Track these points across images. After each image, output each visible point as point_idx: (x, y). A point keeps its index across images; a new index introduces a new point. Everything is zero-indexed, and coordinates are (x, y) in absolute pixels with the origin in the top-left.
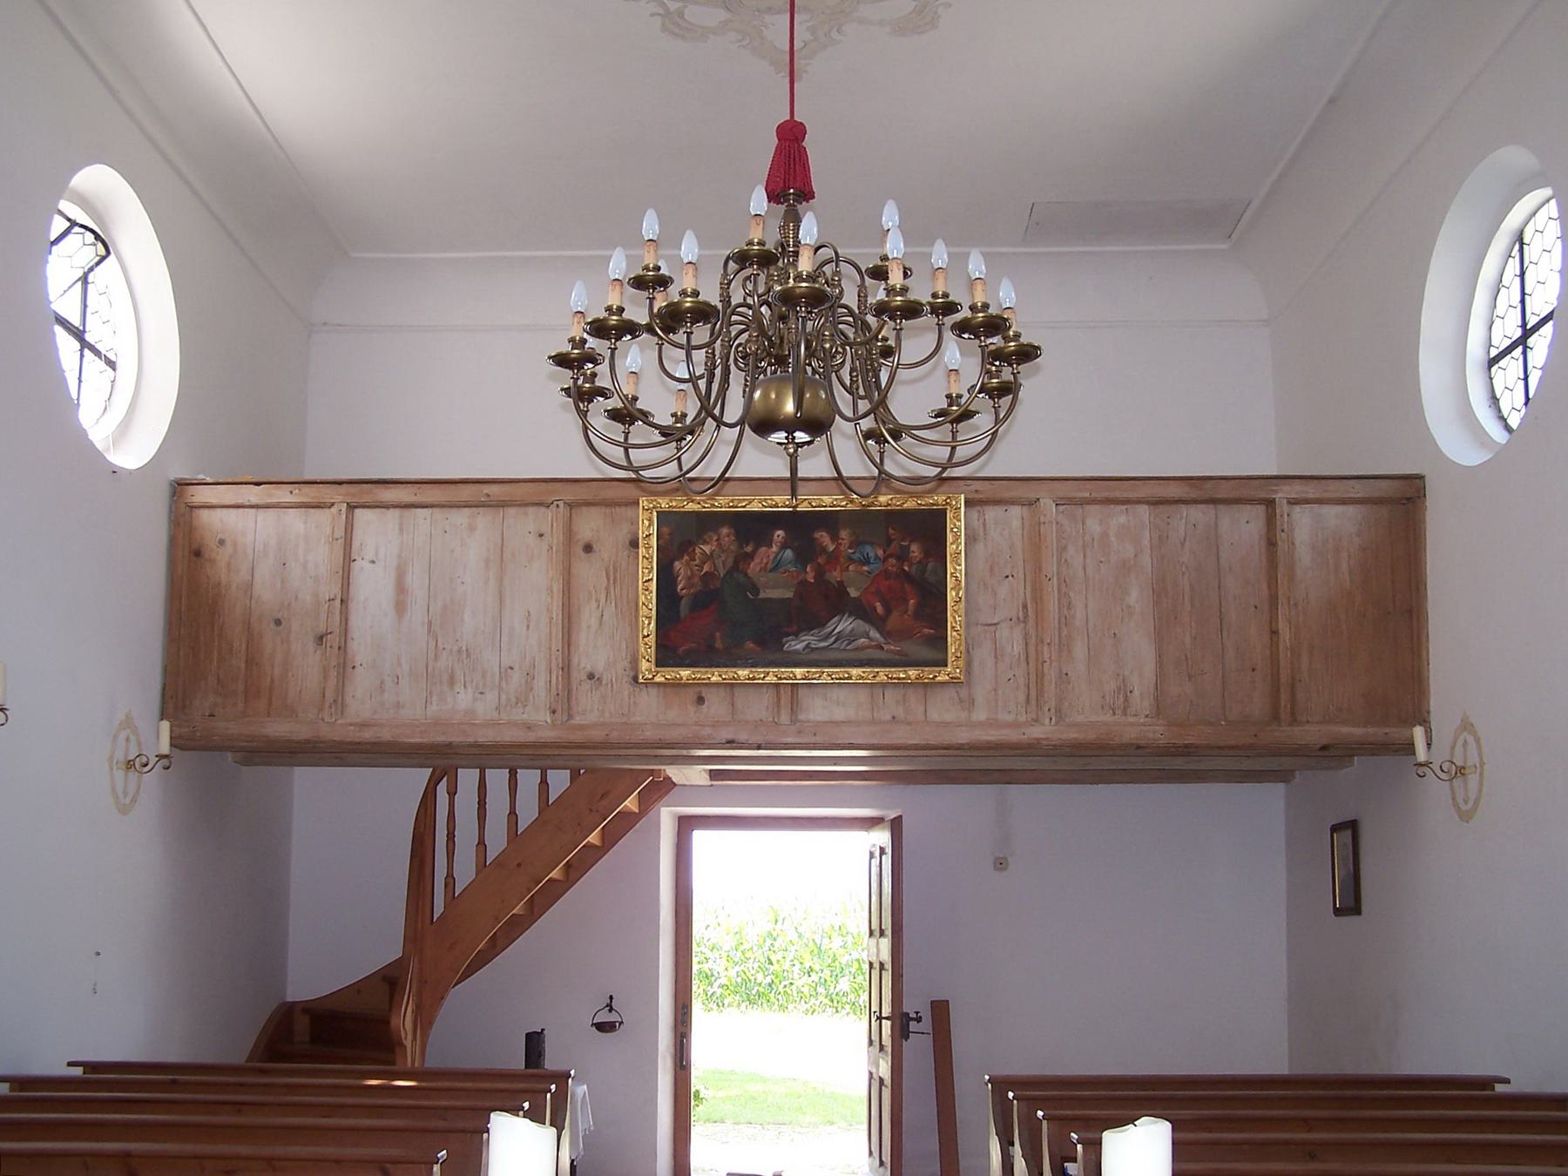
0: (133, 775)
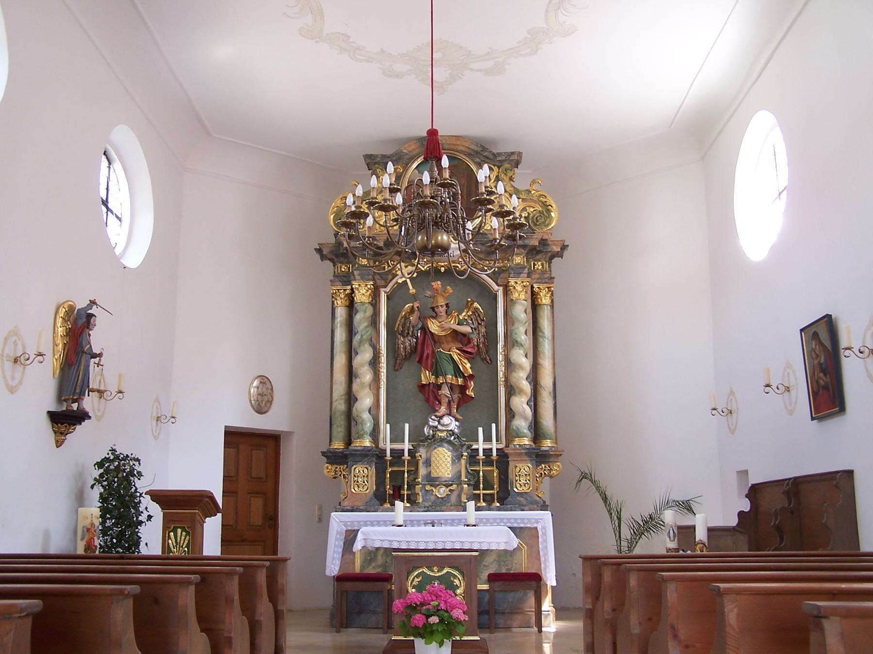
0: (19, 368)
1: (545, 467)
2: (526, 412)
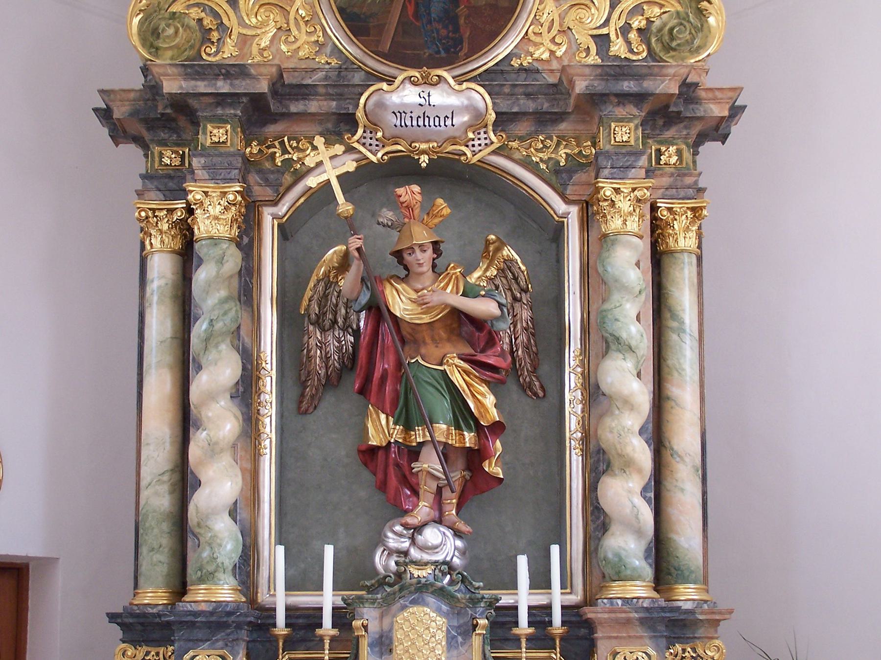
1: (684, 651)
2: (640, 517)
